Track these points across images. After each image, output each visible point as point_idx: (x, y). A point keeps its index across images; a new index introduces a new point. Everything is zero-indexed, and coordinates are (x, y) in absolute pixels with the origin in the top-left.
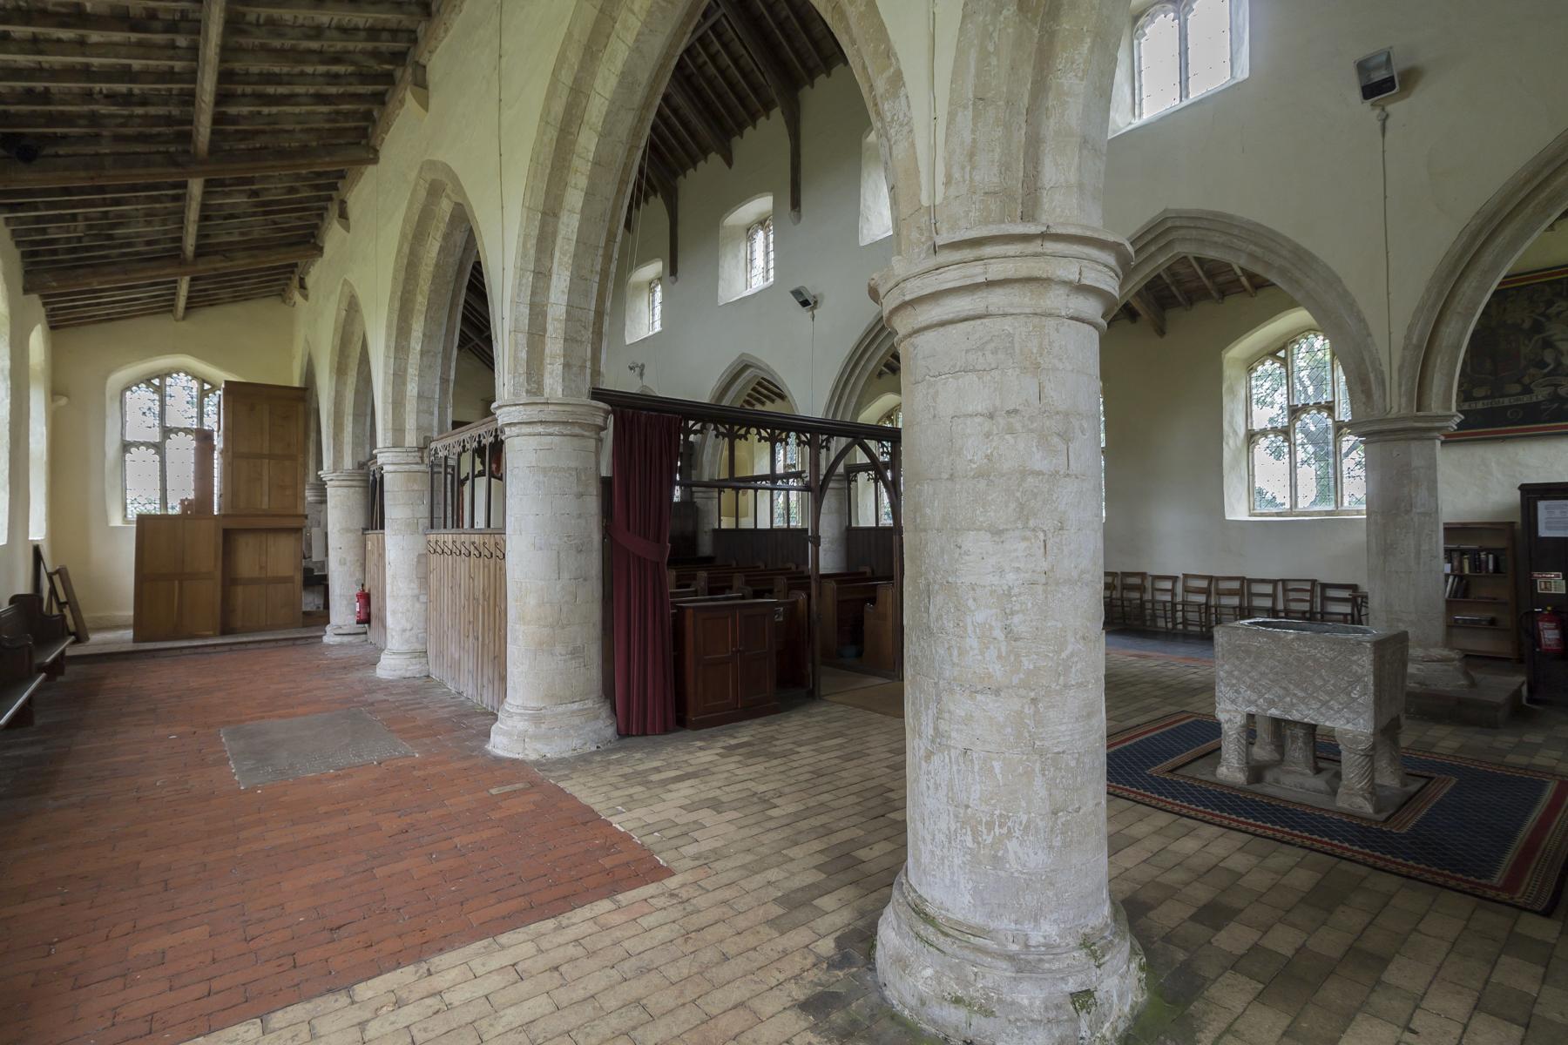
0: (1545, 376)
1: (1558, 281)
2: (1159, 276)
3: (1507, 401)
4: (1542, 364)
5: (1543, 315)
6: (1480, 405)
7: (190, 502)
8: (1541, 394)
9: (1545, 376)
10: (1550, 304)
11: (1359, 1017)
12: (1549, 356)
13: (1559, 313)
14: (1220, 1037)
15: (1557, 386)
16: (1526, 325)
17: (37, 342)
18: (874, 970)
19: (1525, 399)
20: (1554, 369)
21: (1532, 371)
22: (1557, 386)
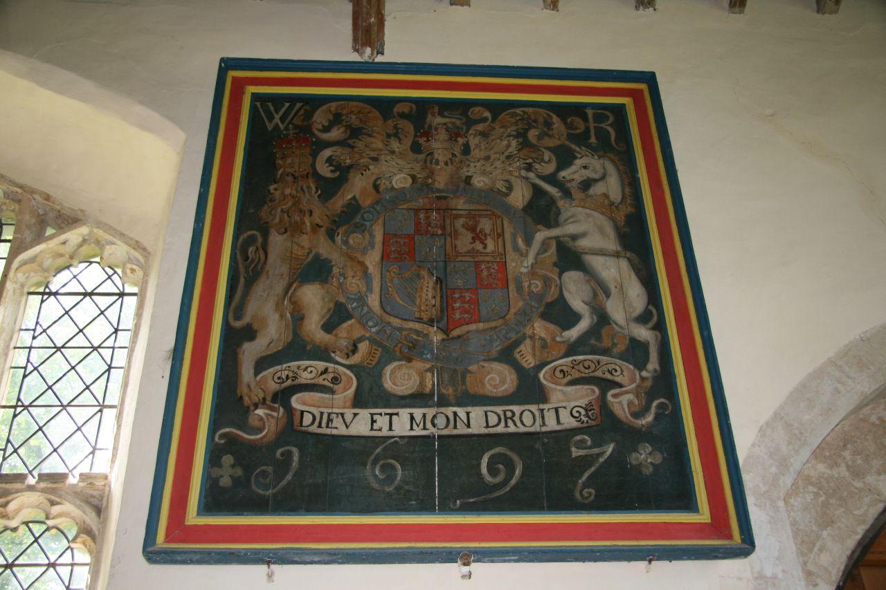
0: (572, 349)
1: (579, 109)
2: (272, 511)
3: (477, 420)
4: (561, 315)
5: (552, 179)
6: (402, 424)
7: (640, 472)
8: (565, 407)
9: (572, 349)
10: (565, 158)
11: (351, 171)
12: (576, 292)
13: (586, 185)
14: (310, 412)
15: (606, 385)
16: (519, 197)
17: (104, 504)
18: (463, 335)
19: (526, 419)
20: (594, 331)
21: (540, 328)
22: (606, 385)
